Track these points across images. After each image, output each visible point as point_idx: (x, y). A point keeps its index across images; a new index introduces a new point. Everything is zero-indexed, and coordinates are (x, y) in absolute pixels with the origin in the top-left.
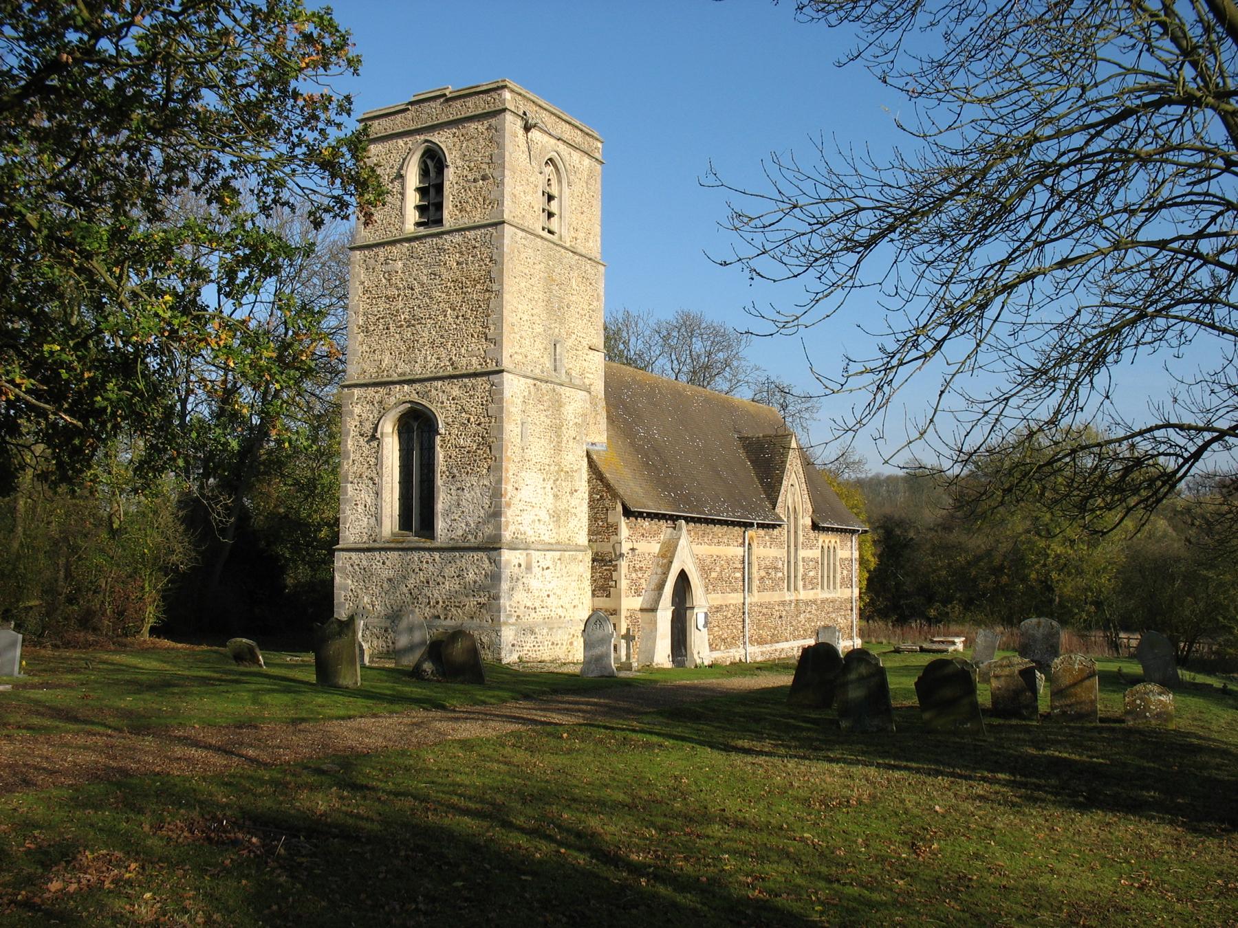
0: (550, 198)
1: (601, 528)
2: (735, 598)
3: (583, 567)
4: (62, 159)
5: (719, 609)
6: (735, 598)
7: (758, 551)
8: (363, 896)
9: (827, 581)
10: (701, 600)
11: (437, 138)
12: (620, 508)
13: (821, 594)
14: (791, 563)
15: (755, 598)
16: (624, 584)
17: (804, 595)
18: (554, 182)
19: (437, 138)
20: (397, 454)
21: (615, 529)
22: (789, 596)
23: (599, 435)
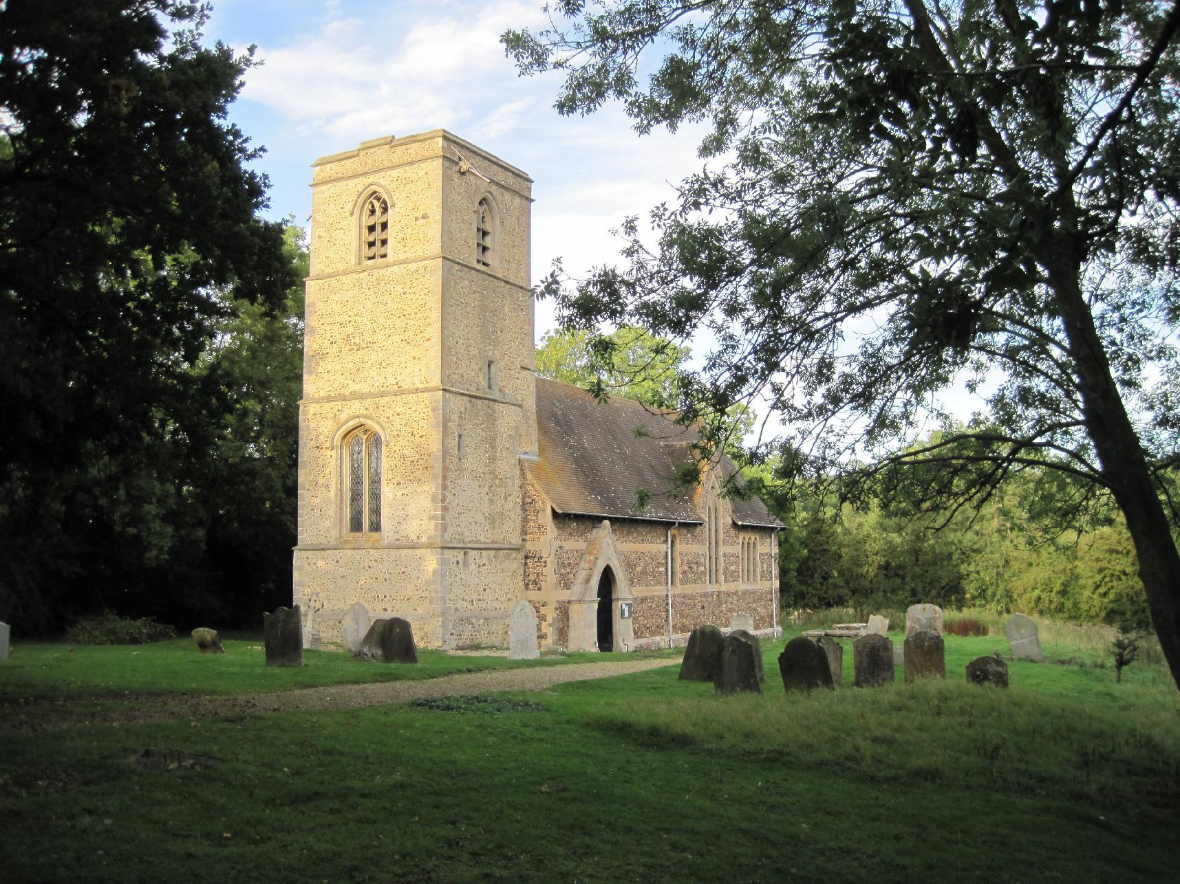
2: (659, 591)
5: (644, 600)
9: (750, 575)
10: (623, 591)
12: (549, 511)
13: (741, 586)
17: (724, 587)
22: (711, 588)
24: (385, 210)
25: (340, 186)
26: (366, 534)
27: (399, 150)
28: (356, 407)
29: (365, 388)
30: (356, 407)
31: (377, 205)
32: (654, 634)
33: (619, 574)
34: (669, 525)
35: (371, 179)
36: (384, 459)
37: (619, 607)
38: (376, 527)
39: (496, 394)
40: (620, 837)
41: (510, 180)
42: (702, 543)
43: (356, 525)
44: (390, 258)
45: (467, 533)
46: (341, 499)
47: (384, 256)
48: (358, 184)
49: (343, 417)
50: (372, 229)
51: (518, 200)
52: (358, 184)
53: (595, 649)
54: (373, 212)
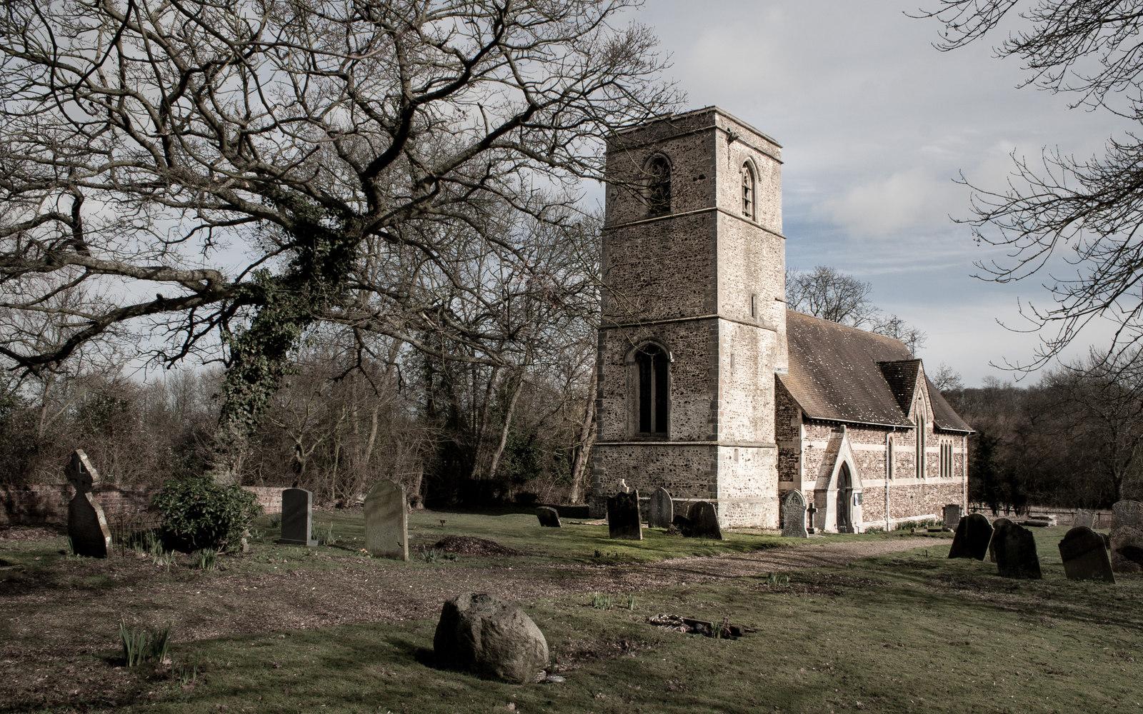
3: (772, 457)
5: (869, 490)
12: (800, 417)
21: (796, 432)
41: (764, 145)
43: (644, 425)
51: (771, 162)
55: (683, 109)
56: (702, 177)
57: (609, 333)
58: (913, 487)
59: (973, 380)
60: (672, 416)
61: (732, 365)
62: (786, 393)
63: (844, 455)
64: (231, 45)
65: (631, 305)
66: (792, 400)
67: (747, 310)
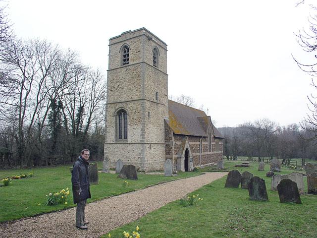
0: (155, 58)
1: (167, 138)
2: (198, 154)
3: (163, 148)
4: (76, 118)
5: (195, 156)
6: (198, 154)
7: (203, 143)
8: (202, 199)
9: (217, 150)
10: (191, 155)
11: (127, 42)
12: (172, 133)
13: (215, 152)
14: (210, 146)
15: (203, 154)
16: (173, 152)
17: (212, 153)
18: (156, 55)
19: (127, 42)
20: (153, 189)
21: (171, 138)
22: (209, 153)
23: (167, 117)
24: (128, 51)
25: (116, 45)
26: (123, 141)
27: (132, 34)
28: (121, 105)
29: (123, 100)
30: (121, 105)
31: (126, 50)
32: (197, 165)
33: (190, 150)
34: (200, 137)
35: (125, 42)
36: (128, 119)
37: (190, 159)
38: (126, 138)
39: (158, 102)
40: (33, 96)
41: (162, 44)
42: (203, 145)
43: (121, 138)
44: (130, 64)
45: (151, 140)
46: (117, 130)
47: (128, 63)
48: (122, 44)
49: (117, 107)
50: (124, 60)
51: (163, 50)
52: (122, 44)
53: (184, 171)
54: (125, 52)
55: (215, 126)
56: (139, 51)
57: (109, 105)
58: (208, 155)
59: (227, 116)
60: (129, 134)
61: (149, 116)
62: (168, 126)
63: (187, 146)
64: (87, 128)
65: (115, 98)
66: (170, 128)
67: (154, 97)
